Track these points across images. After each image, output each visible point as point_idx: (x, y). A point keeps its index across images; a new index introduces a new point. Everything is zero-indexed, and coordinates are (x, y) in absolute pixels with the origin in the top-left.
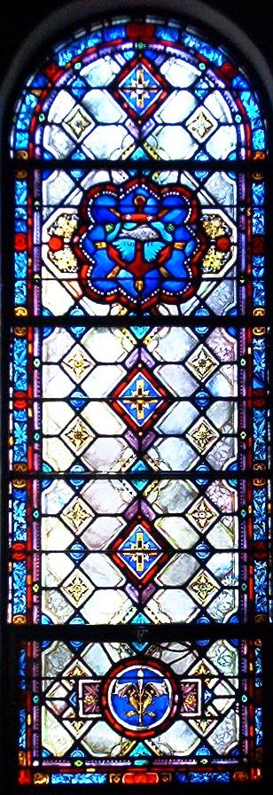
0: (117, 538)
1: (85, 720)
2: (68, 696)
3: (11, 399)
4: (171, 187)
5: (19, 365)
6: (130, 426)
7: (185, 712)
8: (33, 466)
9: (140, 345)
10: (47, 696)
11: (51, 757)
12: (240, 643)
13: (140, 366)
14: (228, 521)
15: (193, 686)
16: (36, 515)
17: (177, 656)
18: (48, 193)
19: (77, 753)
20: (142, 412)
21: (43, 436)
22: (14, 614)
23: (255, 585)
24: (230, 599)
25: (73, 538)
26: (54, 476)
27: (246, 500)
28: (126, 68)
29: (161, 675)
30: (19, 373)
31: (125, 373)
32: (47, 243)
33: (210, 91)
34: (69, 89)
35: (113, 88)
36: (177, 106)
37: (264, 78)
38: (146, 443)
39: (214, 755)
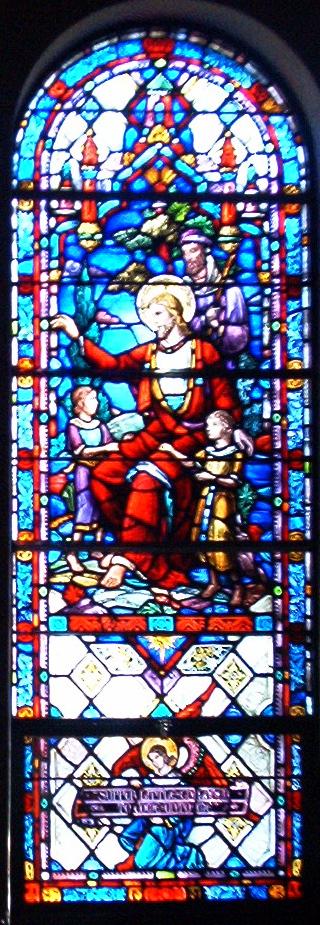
0: (137, 651)
8: (40, 712)
9: (161, 696)
12: (276, 739)
18: (56, 769)
21: (50, 676)
22: (19, 701)
25: (88, 852)
32: (42, 424)
33: (240, 114)
37: (312, 125)
39: (247, 867)
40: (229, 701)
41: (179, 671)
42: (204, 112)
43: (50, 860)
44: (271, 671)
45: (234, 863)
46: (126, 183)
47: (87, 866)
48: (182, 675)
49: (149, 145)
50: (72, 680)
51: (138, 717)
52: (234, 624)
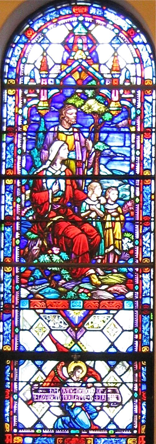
3: (4, 132)
5: (7, 289)
9: (76, 340)
16: (17, 330)
23: (143, 241)
33: (121, 44)
40: (110, 344)
41: (85, 328)
43: (18, 423)
45: (112, 427)
46: (64, 79)
47: (109, 427)
48: (86, 330)
49: (74, 61)
51: (92, 351)
52: (59, 304)
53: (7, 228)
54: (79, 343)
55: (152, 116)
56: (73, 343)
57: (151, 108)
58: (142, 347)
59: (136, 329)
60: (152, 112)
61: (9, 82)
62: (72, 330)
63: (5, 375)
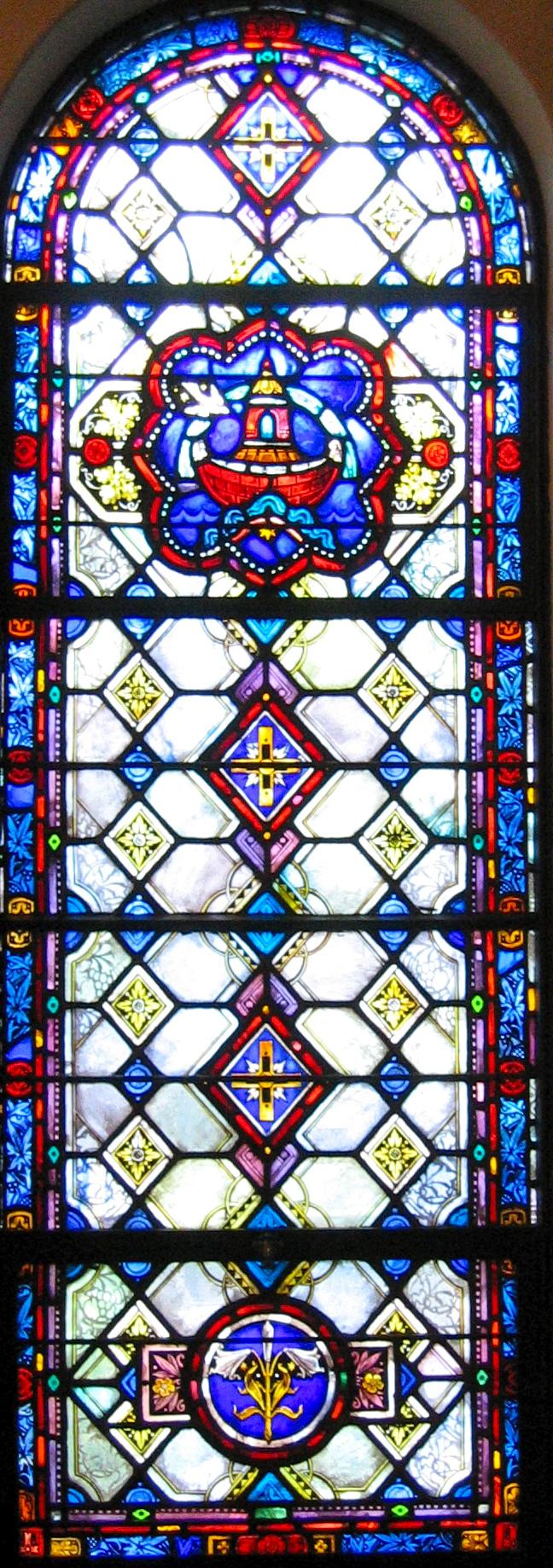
1: (155, 1427)
2: (120, 1376)
4: (329, 338)
6: (248, 822)
7: (363, 1409)
9: (269, 248)
10: (77, 1376)
11: (89, 1505)
13: (267, 836)
14: (442, 1014)
15: (376, 1356)
16: (54, 1154)
17: (344, 1294)
19: (139, 1495)
20: (271, 1105)
23: (498, 837)
24: (448, 1177)
26: (90, 922)
27: (484, 662)
28: (236, 106)
29: (313, 1334)
30: (17, 859)
31: (235, 1023)
34: (127, 143)
35: (215, 141)
36: (344, 179)
38: (278, 1171)
39: (423, 1496)
42: (347, 144)
44: (462, 686)
50: (121, 194)
53: (15, 1104)
54: (278, 256)
55: (526, 710)
56: (256, 886)
57: (518, 681)
58: (500, 1208)
59: (476, 689)
60: (523, 693)
61: (20, 275)
62: (251, 840)
63: (17, 1325)
